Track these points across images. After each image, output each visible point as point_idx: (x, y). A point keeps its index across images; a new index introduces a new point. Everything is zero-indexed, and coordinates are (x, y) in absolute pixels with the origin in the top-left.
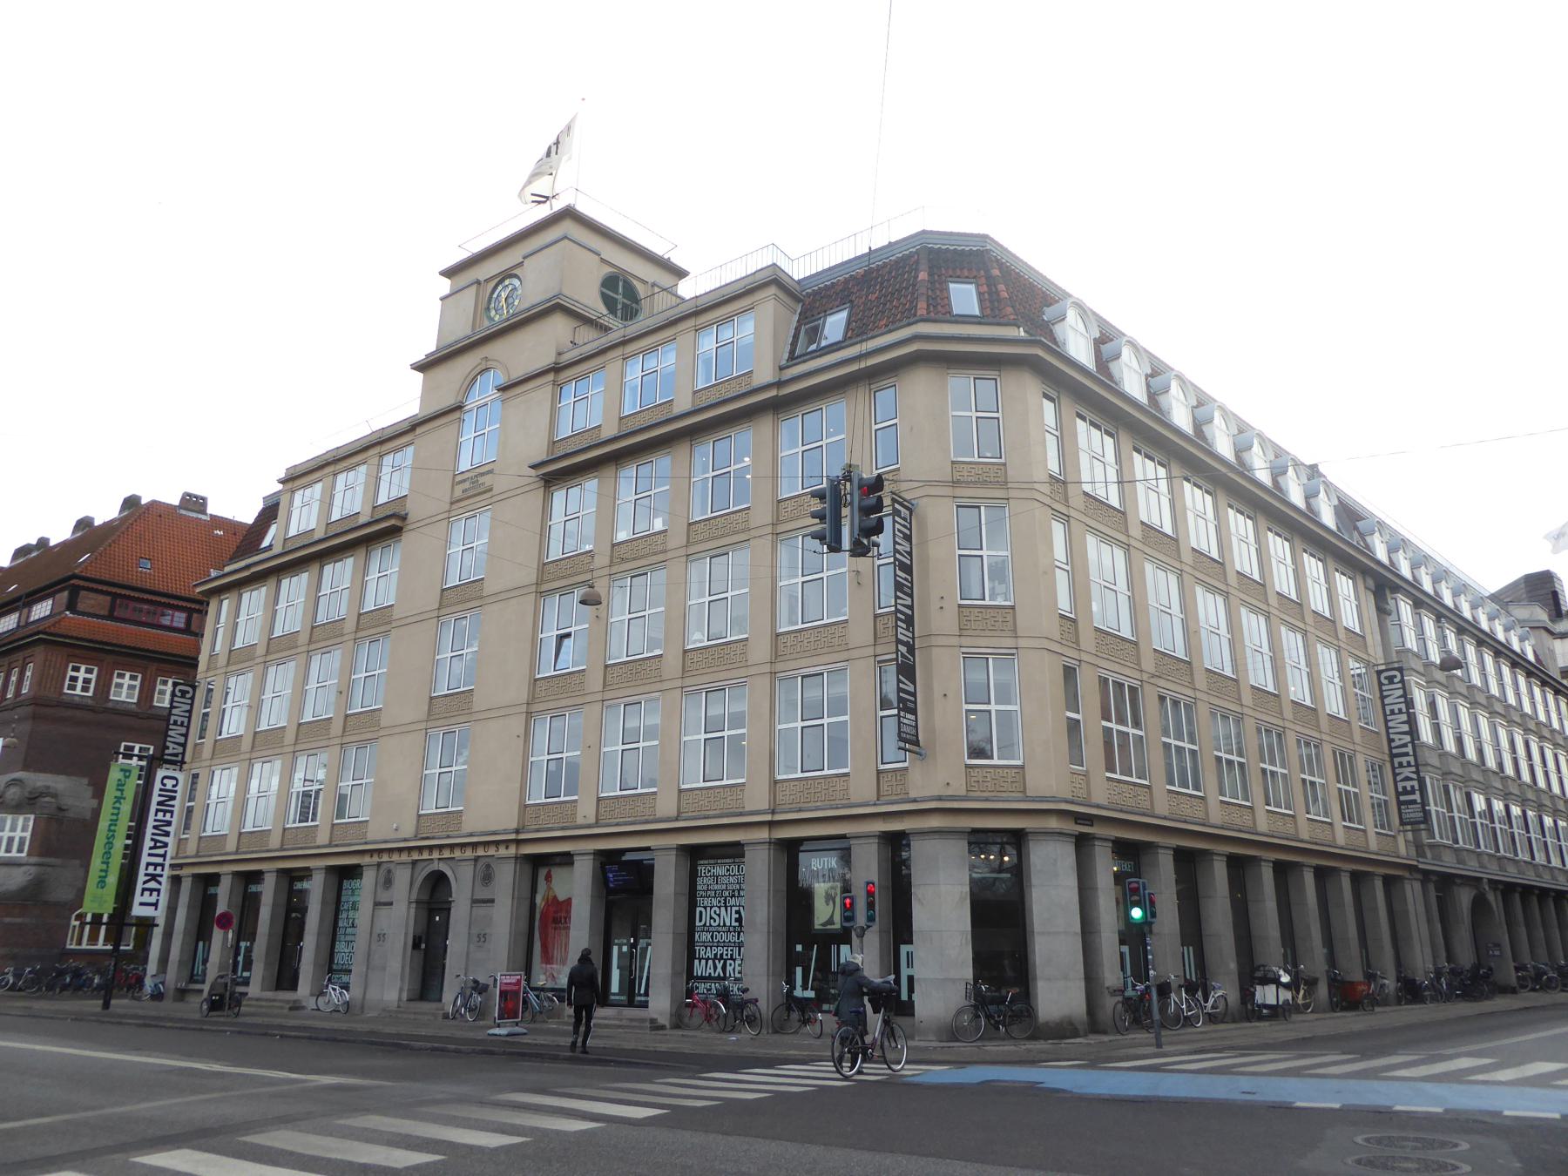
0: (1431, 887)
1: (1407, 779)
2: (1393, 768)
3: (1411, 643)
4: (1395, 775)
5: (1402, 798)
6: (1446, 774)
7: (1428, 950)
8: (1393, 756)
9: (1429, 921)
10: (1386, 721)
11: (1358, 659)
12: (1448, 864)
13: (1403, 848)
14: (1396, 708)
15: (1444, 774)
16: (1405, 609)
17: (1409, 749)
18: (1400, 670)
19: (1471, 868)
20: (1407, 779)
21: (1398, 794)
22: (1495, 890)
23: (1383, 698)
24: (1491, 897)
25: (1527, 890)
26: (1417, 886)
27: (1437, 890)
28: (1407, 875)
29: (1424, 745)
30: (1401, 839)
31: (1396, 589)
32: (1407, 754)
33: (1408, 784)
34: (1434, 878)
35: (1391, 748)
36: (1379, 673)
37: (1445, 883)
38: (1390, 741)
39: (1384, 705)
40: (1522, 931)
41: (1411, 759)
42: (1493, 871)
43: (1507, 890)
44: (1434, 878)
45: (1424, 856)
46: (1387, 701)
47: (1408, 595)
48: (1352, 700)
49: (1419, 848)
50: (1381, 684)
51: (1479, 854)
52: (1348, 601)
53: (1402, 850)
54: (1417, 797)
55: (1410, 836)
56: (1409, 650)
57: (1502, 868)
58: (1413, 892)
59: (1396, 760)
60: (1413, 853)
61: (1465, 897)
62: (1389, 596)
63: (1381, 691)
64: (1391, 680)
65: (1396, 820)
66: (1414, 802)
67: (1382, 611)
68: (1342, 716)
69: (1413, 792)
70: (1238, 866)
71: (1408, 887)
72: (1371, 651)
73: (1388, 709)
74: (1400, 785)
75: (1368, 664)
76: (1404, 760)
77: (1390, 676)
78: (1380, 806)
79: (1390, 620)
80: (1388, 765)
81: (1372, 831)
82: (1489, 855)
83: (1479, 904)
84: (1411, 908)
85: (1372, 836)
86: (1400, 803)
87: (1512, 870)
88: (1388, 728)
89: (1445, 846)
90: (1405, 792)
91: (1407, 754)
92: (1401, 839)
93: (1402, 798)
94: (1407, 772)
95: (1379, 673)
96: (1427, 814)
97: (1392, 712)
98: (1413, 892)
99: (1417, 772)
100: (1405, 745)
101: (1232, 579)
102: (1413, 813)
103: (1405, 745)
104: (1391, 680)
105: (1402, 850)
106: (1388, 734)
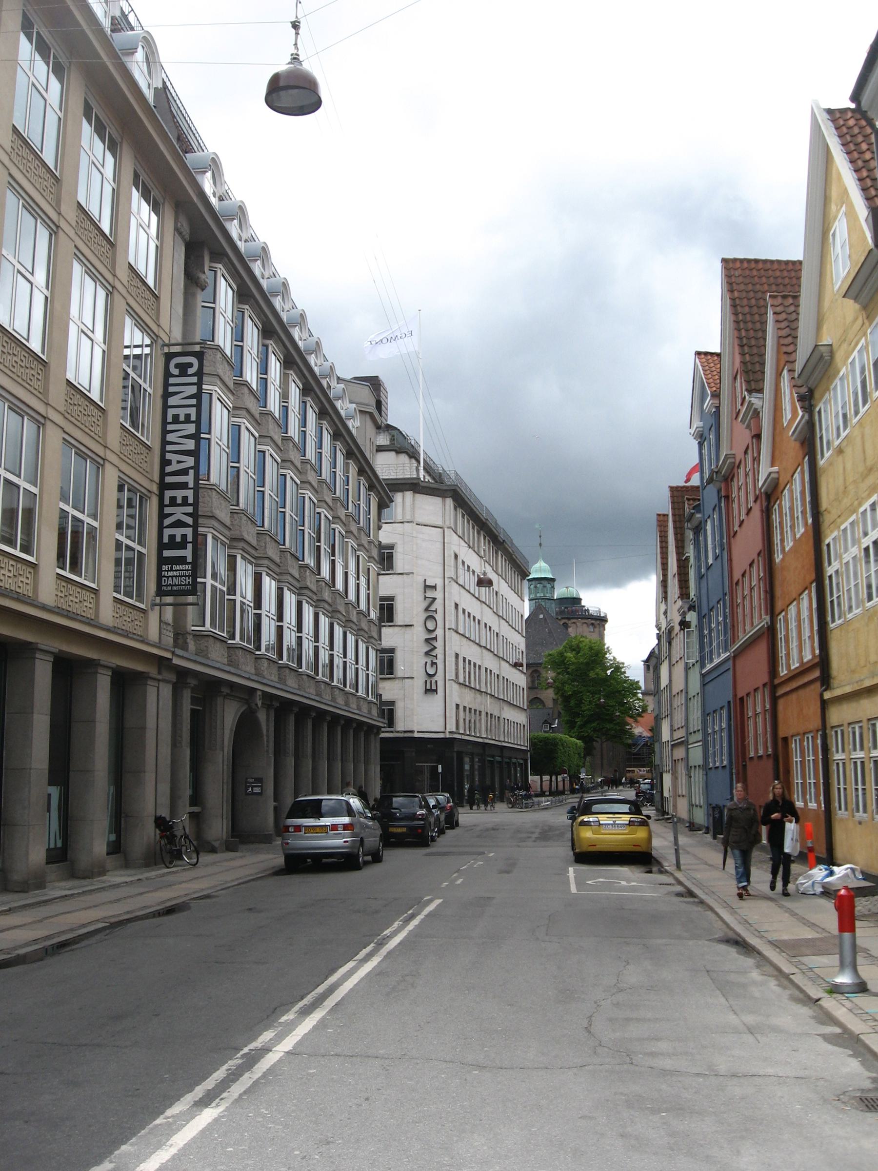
0: (187, 695)
1: (179, 524)
2: (162, 506)
3: (224, 338)
4: (162, 516)
5: (167, 553)
6: (236, 541)
7: (165, 788)
8: (163, 486)
9: (175, 743)
10: (165, 432)
11: (144, 327)
12: (215, 664)
13: (153, 629)
14: (182, 412)
15: (232, 539)
16: (225, 295)
17: (190, 479)
18: (200, 356)
19: (244, 674)
20: (179, 524)
21: (161, 546)
22: (268, 707)
23: (166, 395)
24: (262, 716)
25: (304, 711)
26: (166, 691)
27: (194, 701)
28: (152, 671)
29: (213, 488)
30: (153, 618)
31: (218, 255)
32: (184, 486)
33: (178, 532)
34: (193, 682)
35: (163, 474)
36: (169, 357)
37: (209, 690)
38: (164, 463)
39: (165, 407)
40: (290, 761)
41: (190, 493)
42: (270, 683)
43: (282, 708)
44: (193, 682)
45: (185, 648)
46: (172, 401)
47: (234, 273)
48: (117, 381)
49: (180, 636)
50: (167, 374)
51: (258, 658)
52: (144, 236)
53: (153, 633)
54: (188, 553)
55: (169, 613)
56: (218, 348)
57: (282, 680)
58: (158, 703)
59: (168, 494)
60: (169, 640)
61: (229, 714)
62: (207, 264)
63: (166, 385)
64: (183, 372)
65: (150, 586)
66: (182, 560)
67: (193, 280)
68: (95, 395)
69: (182, 545)
70: (68, 670)
71: (151, 692)
72: (164, 321)
73: (171, 412)
74: (167, 532)
75: (155, 338)
76: (179, 494)
77: (187, 362)
78: (128, 565)
79: (200, 297)
80: (155, 501)
81: (108, 594)
82: (269, 660)
83: (246, 727)
84: (151, 722)
85: (106, 602)
86: (162, 561)
87: (292, 682)
88: (164, 443)
89: (216, 638)
90: (173, 544)
91: (184, 486)
92: (153, 618)
93: (167, 553)
94: (179, 513)
95: (169, 357)
96: (194, 589)
97: (176, 419)
98: (158, 703)
99: (195, 515)
100: (184, 472)
101: (57, 394)
102: (177, 575)
103: (184, 472)
104: (183, 369)
105: (153, 633)
106: (163, 452)
